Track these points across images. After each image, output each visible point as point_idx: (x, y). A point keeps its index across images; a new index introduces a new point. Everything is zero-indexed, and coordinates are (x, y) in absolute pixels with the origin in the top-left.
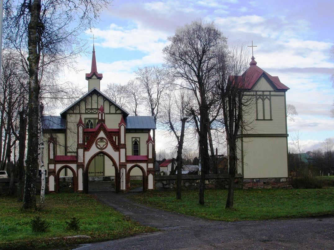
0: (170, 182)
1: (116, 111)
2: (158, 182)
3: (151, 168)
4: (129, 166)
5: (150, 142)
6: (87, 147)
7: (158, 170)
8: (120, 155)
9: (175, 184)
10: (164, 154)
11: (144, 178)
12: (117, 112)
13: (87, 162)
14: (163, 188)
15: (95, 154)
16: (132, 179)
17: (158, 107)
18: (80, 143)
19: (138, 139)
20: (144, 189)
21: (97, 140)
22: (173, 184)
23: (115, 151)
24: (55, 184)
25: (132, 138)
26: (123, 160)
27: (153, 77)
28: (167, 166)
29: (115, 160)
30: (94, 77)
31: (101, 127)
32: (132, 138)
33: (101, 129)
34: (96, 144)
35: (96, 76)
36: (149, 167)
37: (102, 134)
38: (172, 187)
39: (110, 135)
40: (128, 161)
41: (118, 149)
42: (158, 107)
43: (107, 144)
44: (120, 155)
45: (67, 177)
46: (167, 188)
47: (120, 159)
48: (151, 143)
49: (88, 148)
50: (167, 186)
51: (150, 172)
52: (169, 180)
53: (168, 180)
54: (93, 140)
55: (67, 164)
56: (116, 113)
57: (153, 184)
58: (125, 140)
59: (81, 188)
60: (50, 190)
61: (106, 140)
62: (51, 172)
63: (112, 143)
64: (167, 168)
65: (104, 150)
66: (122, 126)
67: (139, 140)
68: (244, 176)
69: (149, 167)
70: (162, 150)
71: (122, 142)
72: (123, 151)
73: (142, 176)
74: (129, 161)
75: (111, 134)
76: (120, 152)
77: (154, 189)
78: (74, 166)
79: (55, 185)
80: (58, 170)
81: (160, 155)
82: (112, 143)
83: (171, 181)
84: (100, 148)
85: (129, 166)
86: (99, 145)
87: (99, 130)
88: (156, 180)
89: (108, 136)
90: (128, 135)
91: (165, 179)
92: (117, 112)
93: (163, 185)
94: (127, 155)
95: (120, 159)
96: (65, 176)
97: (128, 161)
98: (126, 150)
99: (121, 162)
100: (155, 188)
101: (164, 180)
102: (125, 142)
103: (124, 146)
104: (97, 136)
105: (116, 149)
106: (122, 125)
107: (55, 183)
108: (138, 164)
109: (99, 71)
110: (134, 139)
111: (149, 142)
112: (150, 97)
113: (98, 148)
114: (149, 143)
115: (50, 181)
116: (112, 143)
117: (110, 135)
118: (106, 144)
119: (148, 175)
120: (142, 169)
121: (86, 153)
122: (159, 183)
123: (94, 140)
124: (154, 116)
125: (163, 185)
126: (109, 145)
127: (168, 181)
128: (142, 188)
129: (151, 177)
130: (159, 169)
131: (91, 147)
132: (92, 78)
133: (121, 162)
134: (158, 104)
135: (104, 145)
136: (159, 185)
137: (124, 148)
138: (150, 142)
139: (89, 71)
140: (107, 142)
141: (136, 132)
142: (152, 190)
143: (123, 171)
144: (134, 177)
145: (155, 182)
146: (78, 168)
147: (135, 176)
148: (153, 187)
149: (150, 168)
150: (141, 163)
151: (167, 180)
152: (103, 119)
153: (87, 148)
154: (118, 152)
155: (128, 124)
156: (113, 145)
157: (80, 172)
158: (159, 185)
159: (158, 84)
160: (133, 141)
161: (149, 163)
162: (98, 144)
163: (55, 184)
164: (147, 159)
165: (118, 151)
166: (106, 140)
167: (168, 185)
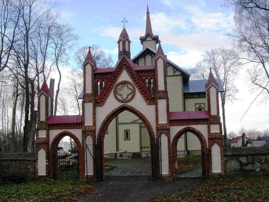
0: (253, 158)
1: (174, 72)
2: (230, 159)
3: (216, 133)
4: (175, 130)
5: (212, 85)
6: (100, 99)
7: (229, 145)
8: (157, 111)
9: (264, 163)
10: (233, 133)
11: (203, 154)
12: (176, 74)
13: (100, 125)
14: (242, 170)
15: (113, 111)
16: (197, 155)
17: (226, 86)
18: (87, 92)
19: (203, 105)
20: (204, 172)
22: (260, 162)
23: (149, 104)
24: (47, 163)
25: (196, 104)
26: (163, 120)
27: (219, 58)
28: (237, 142)
29: (149, 120)
30: (149, 38)
31: (122, 64)
32: (196, 104)
33: (122, 67)
34: (115, 93)
35: (151, 37)
36: (212, 132)
37: (125, 76)
38: (258, 170)
39: (140, 76)
40: (172, 122)
41: (154, 100)
42: (226, 86)
43: (134, 92)
44: (157, 111)
45: (118, 152)
46: (248, 171)
47: (157, 118)
48: (215, 87)
49: (101, 101)
50: (249, 167)
51: (215, 140)
52: (253, 155)
53: (250, 155)
54: (109, 87)
55: (66, 129)
56: (174, 76)
57: (222, 163)
58: (165, 83)
59: (90, 171)
60: (40, 174)
61: (131, 84)
62: (41, 144)
63: (143, 91)
64: (237, 143)
65: (129, 104)
66: (160, 59)
67: (204, 107)
69: (212, 132)
70: (231, 131)
71: (161, 87)
72: (162, 103)
73: (200, 150)
74: (174, 120)
75: (141, 75)
76: (156, 105)
77: (223, 173)
79: (46, 165)
80: (52, 140)
81: (230, 135)
82: (142, 90)
83: (256, 157)
85: (175, 130)
86: (119, 95)
87: (120, 69)
88: (227, 156)
89: (135, 78)
90: (188, 101)
91: (244, 153)
92: (176, 74)
93: (241, 164)
94: (171, 110)
95: (157, 118)
96: (117, 151)
97: (172, 122)
98: (168, 101)
99: (159, 123)
100: (225, 172)
101: (243, 156)
102: (166, 88)
103: (165, 95)
104: (116, 80)
105: (151, 100)
106: (158, 58)
107: (47, 162)
109: (155, 32)
110: (197, 106)
111: (210, 85)
112: (218, 77)
113: (117, 99)
114: (210, 87)
115: (39, 158)
116: (143, 91)
117: (140, 76)
118: (131, 93)
119: (211, 146)
120: (198, 135)
121: (98, 109)
122: (233, 161)
123: (110, 87)
124: (223, 95)
125: (241, 164)
126: (138, 95)
127: (250, 157)
128: (200, 171)
130: (230, 144)
131: (106, 99)
132: (146, 40)
133: (159, 123)
134: (226, 83)
135: (128, 95)
136: (233, 164)
137: (165, 98)
139: (143, 34)
140: (134, 88)
141: (199, 97)
142: (219, 175)
143: (164, 139)
144: (192, 151)
145: (225, 159)
146: (85, 134)
147: (195, 151)
148: (222, 169)
149: (213, 133)
150: (197, 124)
151: (249, 155)
152: (127, 50)
153: (99, 101)
154: (153, 107)
155: (190, 88)
156: (145, 94)
157: (89, 141)
158: (233, 164)
159: (225, 64)
160: (197, 107)
161: (212, 124)
162: (117, 93)
163: (47, 163)
164: (207, 117)
165: (154, 104)
166: (131, 84)
167: (250, 166)
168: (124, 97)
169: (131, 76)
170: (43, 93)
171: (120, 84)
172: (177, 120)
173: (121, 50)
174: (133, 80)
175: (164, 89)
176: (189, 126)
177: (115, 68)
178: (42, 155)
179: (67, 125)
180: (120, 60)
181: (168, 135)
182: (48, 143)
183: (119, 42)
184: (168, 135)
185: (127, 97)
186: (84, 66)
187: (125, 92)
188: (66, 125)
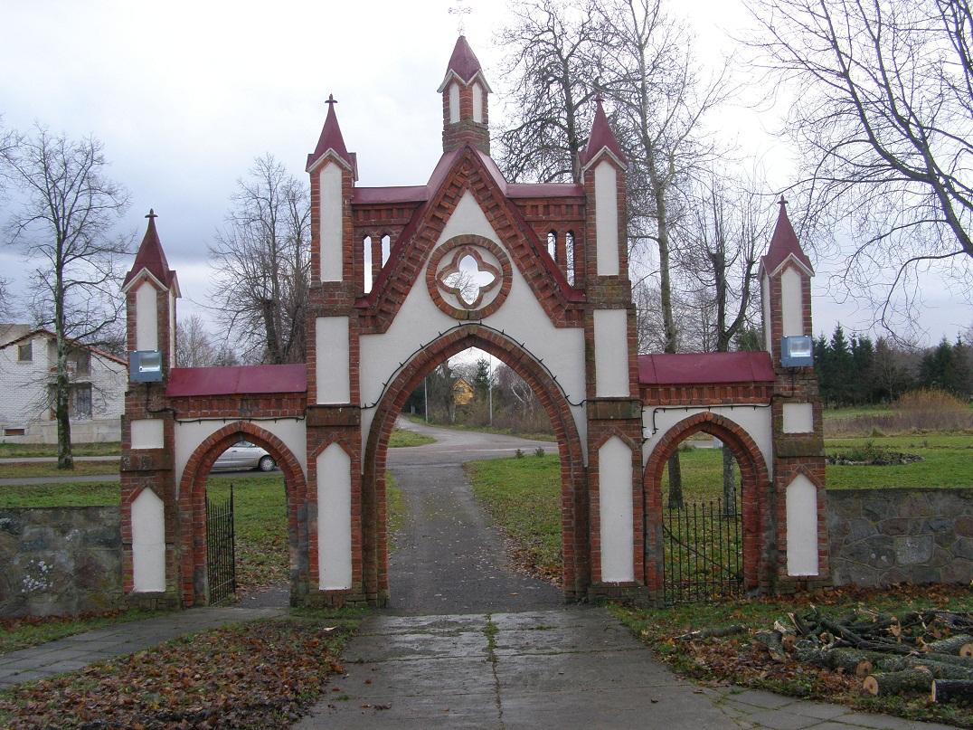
4: (661, 421)
21: (435, 262)
26: (613, 383)
34: (434, 287)
37: (468, 217)
61: (490, 247)
68: (323, 575)
71: (607, 265)
78: (290, 433)
84: (481, 252)
85: (661, 421)
108: (727, 413)
120: (734, 440)
121: (369, 344)
129: (801, 500)
135: (484, 290)
138: (791, 263)
140: (505, 264)
143: (615, 464)
154: (573, 337)
168: (470, 297)
169: (553, 309)
170: (146, 279)
171: (450, 246)
172: (197, 397)
173: (455, 118)
174: (536, 286)
175: (615, 272)
176: (713, 411)
177: (432, 191)
178: (147, 515)
179: (740, 389)
180: (451, 158)
181: (636, 443)
182: (168, 471)
183: (445, 91)
184: (636, 443)
185: (480, 299)
186: (312, 175)
187: (472, 279)
188: (657, 391)
